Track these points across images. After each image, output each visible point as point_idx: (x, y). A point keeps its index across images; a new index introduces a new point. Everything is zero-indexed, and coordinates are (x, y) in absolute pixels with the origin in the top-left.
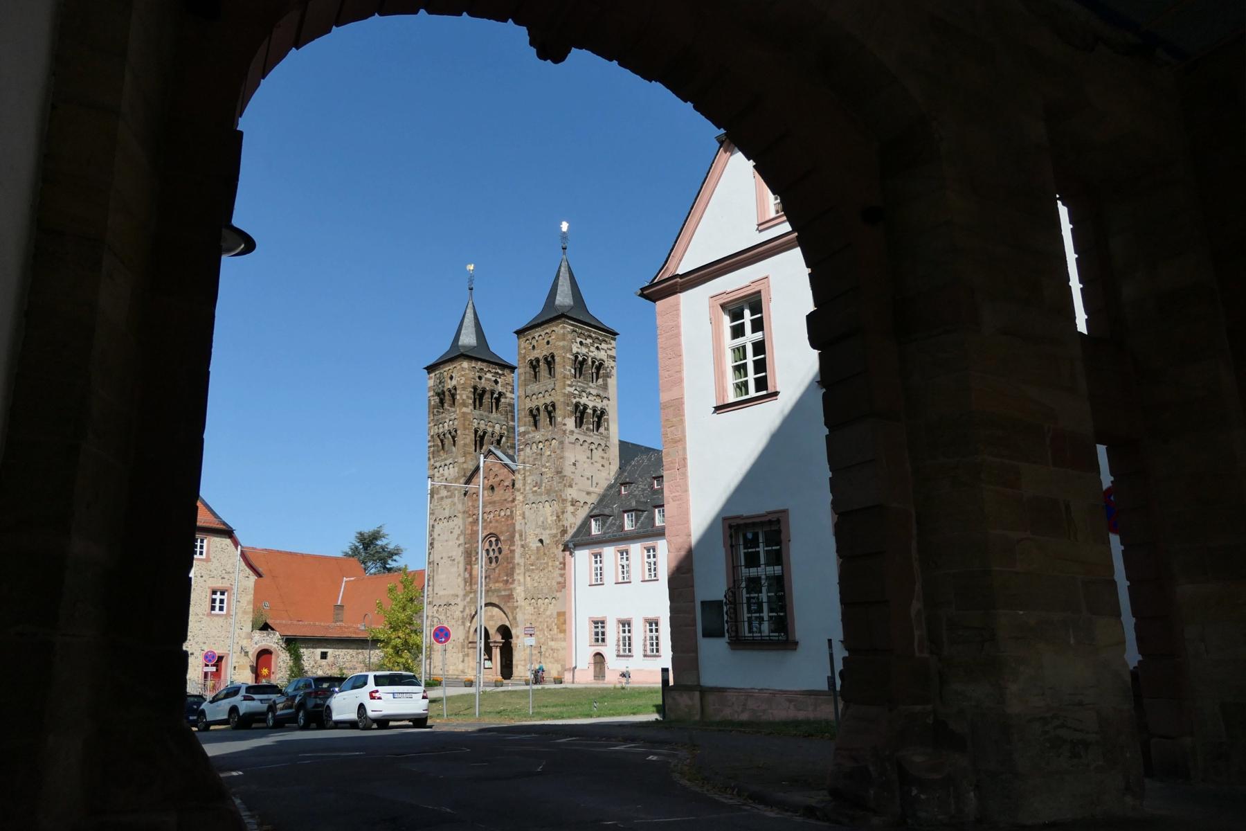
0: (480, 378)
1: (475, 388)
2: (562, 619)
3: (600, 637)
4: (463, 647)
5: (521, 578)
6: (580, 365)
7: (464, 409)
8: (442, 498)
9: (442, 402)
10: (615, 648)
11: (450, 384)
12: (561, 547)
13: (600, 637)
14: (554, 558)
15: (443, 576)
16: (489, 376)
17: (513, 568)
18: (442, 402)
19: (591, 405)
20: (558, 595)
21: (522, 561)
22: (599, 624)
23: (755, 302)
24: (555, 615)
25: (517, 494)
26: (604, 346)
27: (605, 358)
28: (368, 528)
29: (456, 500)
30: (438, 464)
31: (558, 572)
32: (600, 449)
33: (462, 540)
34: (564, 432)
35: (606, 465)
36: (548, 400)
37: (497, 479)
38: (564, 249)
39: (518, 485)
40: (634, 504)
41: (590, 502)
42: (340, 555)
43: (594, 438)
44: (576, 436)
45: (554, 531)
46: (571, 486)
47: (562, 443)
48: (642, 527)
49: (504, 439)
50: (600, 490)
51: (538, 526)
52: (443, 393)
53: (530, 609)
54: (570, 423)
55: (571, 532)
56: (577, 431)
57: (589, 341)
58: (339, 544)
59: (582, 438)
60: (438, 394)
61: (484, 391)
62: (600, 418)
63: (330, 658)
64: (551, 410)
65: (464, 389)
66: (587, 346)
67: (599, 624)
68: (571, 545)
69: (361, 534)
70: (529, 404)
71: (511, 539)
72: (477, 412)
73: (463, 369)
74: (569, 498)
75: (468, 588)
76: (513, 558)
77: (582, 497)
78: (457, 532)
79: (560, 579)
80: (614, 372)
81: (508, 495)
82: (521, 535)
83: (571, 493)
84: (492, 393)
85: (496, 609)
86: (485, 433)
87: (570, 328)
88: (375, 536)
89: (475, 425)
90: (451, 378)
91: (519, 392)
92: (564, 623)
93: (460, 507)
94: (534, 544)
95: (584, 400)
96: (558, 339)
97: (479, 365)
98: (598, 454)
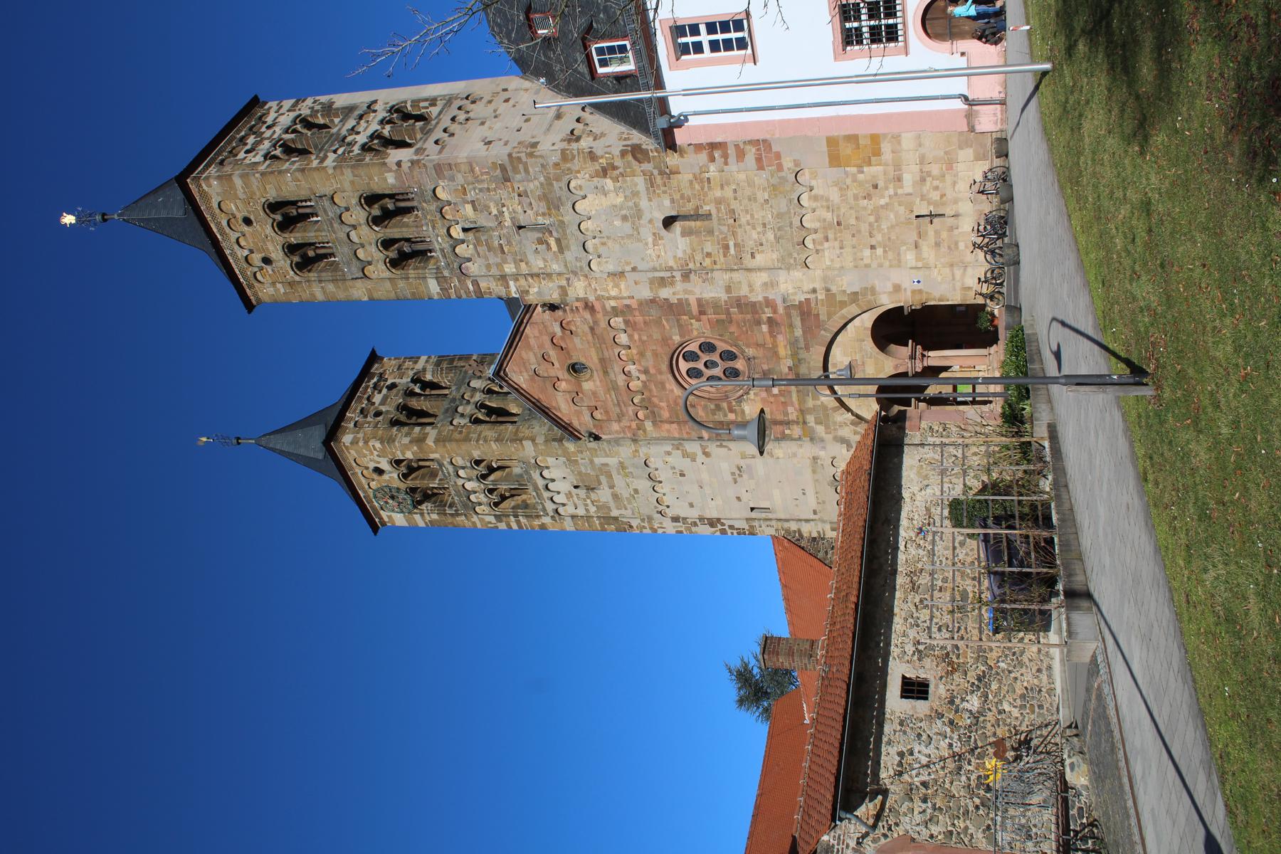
0: (378, 414)
1: (395, 423)
2: (846, 150)
7: (430, 442)
8: (616, 497)
9: (428, 496)
11: (392, 477)
12: (672, 159)
14: (701, 179)
15: (776, 493)
16: (377, 398)
17: (741, 304)
19: (375, 127)
20: (788, 163)
21: (722, 278)
24: (835, 173)
26: (269, 120)
28: (731, 691)
29: (613, 461)
33: (693, 447)
36: (358, 215)
37: (553, 354)
42: (763, 729)
45: (640, 182)
47: (439, 169)
51: (635, 235)
53: (830, 253)
55: (637, 137)
57: (251, 140)
58: (752, 732)
59: (438, 134)
60: (417, 504)
61: (403, 408)
62: (406, 116)
63: (927, 671)
69: (741, 702)
70: (379, 270)
71: (675, 310)
73: (355, 442)
75: (796, 431)
76: (716, 305)
78: (676, 459)
80: (324, 99)
81: (580, 322)
82: (662, 282)
83: (551, 144)
84: (410, 394)
85: (836, 352)
86: (483, 406)
87: (213, 170)
88: (743, 676)
90: (379, 471)
92: (853, 139)
93: (626, 451)
94: (677, 244)
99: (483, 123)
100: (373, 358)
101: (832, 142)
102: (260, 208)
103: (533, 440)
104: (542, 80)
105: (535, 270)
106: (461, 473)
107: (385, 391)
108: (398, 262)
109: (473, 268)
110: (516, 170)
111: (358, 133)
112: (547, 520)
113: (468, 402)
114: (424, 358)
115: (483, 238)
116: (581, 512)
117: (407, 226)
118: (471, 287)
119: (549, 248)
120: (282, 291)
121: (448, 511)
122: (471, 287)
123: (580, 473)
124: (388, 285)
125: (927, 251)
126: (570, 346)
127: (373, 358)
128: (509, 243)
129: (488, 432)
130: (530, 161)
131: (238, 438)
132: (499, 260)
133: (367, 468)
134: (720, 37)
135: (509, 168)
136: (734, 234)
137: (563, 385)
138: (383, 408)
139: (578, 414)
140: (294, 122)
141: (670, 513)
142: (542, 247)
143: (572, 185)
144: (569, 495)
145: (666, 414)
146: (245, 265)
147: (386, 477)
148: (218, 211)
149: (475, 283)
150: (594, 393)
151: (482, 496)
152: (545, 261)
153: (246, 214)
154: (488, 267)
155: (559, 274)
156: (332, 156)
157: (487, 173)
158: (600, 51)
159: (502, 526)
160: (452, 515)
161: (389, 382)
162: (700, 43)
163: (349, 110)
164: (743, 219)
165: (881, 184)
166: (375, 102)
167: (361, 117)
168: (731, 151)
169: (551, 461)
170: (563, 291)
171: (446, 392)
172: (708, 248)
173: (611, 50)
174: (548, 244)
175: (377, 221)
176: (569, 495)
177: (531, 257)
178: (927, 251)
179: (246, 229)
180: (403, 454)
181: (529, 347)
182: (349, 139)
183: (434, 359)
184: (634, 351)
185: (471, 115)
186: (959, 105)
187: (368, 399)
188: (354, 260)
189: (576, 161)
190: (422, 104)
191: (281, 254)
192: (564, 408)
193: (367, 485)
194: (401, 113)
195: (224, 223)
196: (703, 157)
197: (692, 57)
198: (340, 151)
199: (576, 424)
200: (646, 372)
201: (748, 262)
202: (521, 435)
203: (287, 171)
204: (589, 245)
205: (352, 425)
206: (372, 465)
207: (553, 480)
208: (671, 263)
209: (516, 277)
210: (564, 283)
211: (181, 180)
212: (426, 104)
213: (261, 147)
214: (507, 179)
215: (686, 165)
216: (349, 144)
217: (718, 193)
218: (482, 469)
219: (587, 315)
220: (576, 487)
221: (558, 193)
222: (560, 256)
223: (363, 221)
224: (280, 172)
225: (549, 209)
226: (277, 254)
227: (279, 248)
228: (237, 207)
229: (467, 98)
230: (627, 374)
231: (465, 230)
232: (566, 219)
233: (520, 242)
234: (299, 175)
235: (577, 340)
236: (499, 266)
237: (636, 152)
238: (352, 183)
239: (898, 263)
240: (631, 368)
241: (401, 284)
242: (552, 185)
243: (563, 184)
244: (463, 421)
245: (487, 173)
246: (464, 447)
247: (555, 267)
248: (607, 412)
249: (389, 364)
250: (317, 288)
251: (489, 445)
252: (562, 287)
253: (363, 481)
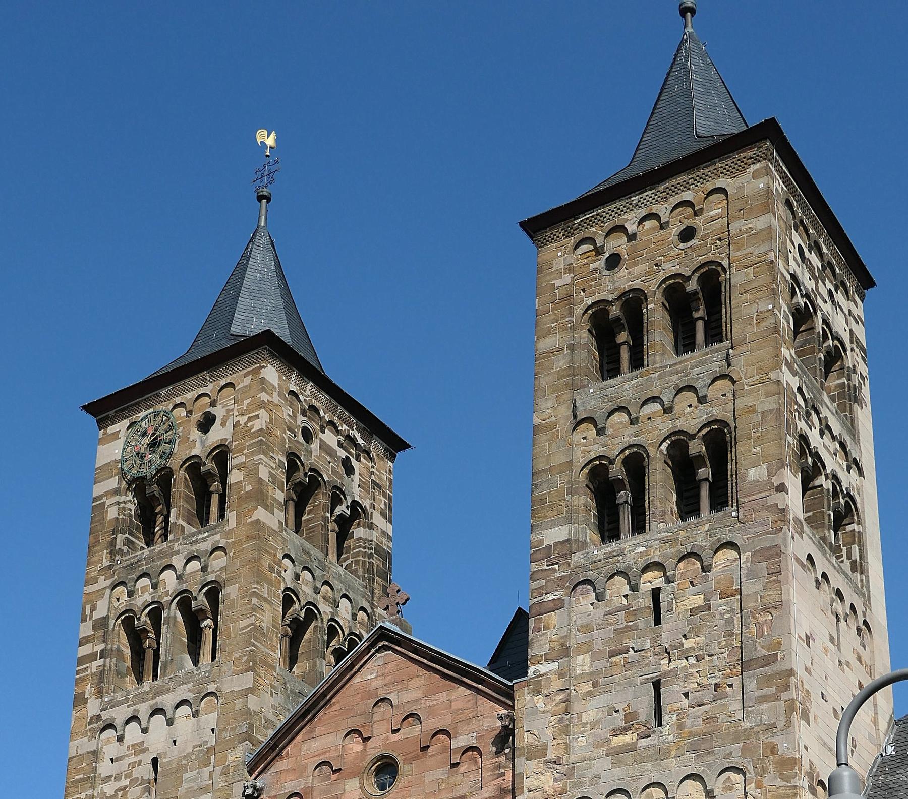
0: (307, 435)
1: (293, 462)
7: (261, 514)
11: (199, 445)
16: (330, 438)
26: (839, 297)
30: (119, 715)
36: (691, 417)
52: (165, 477)
57: (813, 258)
59: (822, 564)
60: (138, 485)
61: (314, 482)
65: (264, 447)
70: (587, 446)
80: (866, 392)
86: (311, 615)
87: (779, 186)
90: (207, 423)
97: (309, 392)
99: (832, 639)
100: (395, 445)
102: (711, 256)
104: (890, 749)
105: (576, 707)
106: (195, 565)
107: (342, 454)
108: (599, 479)
109: (585, 601)
110: (765, 681)
111: (822, 433)
112: (93, 707)
113: (317, 591)
114: (389, 529)
115: (641, 623)
118: (551, 597)
119: (617, 732)
120: (558, 283)
121: (120, 538)
122: (551, 597)
123: (182, 769)
124: (560, 459)
126: (430, 762)
127: (395, 445)
128: (628, 665)
130: (781, 705)
131: (269, 199)
132: (598, 646)
133: (213, 404)
135: (768, 670)
137: (355, 746)
138: (315, 446)
139: (299, 771)
140: (836, 338)
142: (619, 720)
143: (733, 776)
144: (140, 748)
146: (608, 225)
147: (195, 434)
148: (710, 186)
149: (558, 605)
151: (147, 597)
152: (594, 725)
153: (700, 233)
154: (586, 628)
155: (567, 747)
156: (794, 382)
157: (761, 634)
159: (86, 629)
160: (113, 543)
161: (354, 462)
163: (852, 426)
166: (861, 473)
167: (843, 445)
169: (210, 719)
174: (624, 731)
177: (602, 700)
179: (675, 231)
180: (239, 467)
181: (430, 692)
183: (387, 545)
185: (843, 623)
187: (331, 423)
188: (610, 406)
189: (779, 782)
190: (855, 549)
191: (626, 286)
193: (180, 404)
194: (845, 514)
195: (687, 196)
199: (280, 765)
202: (262, 671)
205: (293, 388)
206: (219, 412)
207: (170, 722)
211: (768, 133)
212: (856, 555)
213: (807, 275)
214: (745, 666)
216: (808, 414)
218: (201, 601)
220: (155, 762)
221: (720, 751)
222: (601, 751)
223: (680, 425)
225: (691, 734)
226: (625, 279)
227: (637, 284)
228: (713, 219)
231: (656, 593)
232: (671, 762)
233: (631, 684)
234: (769, 323)
235: (441, 773)
236: (587, 647)
238: (752, 410)
241: (561, 481)
242: (736, 740)
243: (737, 760)
244: (288, 576)
245: (761, 634)
246: (245, 571)
247: (581, 743)
249: (383, 469)
250: (565, 342)
251: (252, 615)
252: (544, 750)
253: (190, 395)
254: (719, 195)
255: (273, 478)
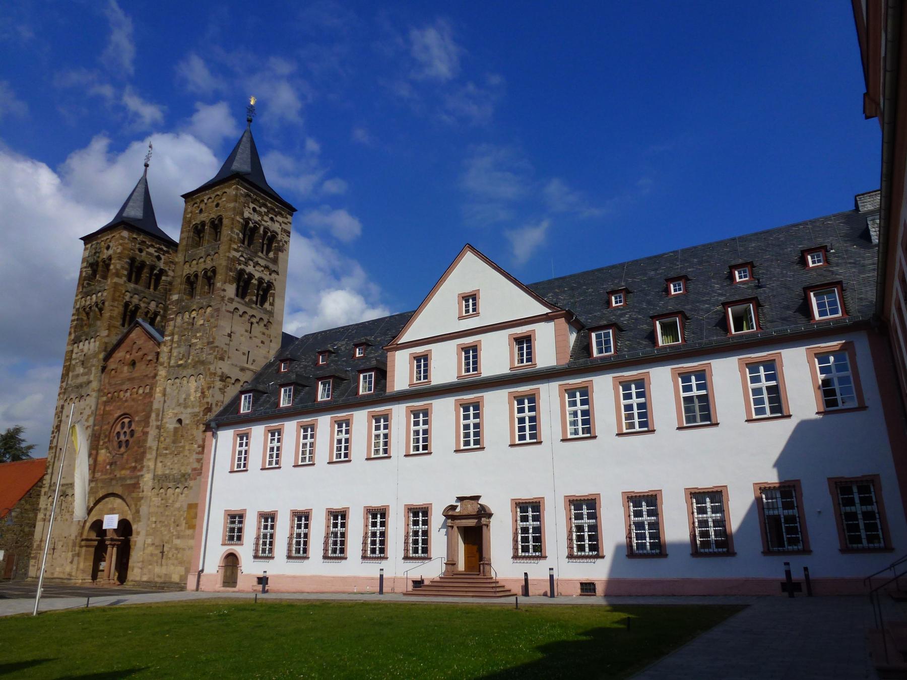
1: (133, 260)
3: (234, 534)
4: (74, 545)
5: (151, 464)
6: (249, 232)
7: (116, 280)
8: (78, 376)
9: (95, 273)
10: (253, 547)
11: (105, 254)
12: (202, 428)
13: (234, 534)
14: (193, 440)
16: (151, 250)
17: (144, 453)
18: (95, 273)
22: (236, 519)
23: (386, 418)
25: (160, 368)
26: (279, 218)
27: (279, 231)
31: (195, 456)
32: (262, 324)
33: (91, 420)
34: (223, 298)
35: (267, 342)
36: (209, 264)
37: (140, 353)
38: (250, 121)
39: (163, 358)
40: (294, 377)
41: (243, 379)
43: (256, 311)
44: (235, 305)
45: (197, 410)
46: (222, 359)
47: (218, 310)
48: (301, 401)
49: (159, 318)
50: (257, 367)
53: (156, 500)
54: (231, 290)
55: (216, 410)
56: (237, 299)
57: (263, 210)
59: (242, 309)
61: (143, 264)
64: (210, 277)
66: (260, 214)
67: (236, 519)
68: (213, 425)
70: (187, 270)
71: (146, 421)
72: (132, 285)
73: (123, 238)
74: (219, 372)
76: (145, 441)
77: (235, 374)
78: (88, 412)
79: (196, 465)
81: (150, 371)
82: (158, 415)
83: (224, 367)
85: (119, 501)
87: (243, 191)
89: (127, 298)
90: (108, 248)
91: (179, 268)
92: (195, 517)
94: (171, 425)
95: (250, 269)
96: (228, 201)
97: (141, 238)
98: (258, 329)
101: (196, 505)
103: (108, 336)
107: (156, 254)
116: (74, 356)
117: (202, 288)
125: (150, 549)
129: (118, 310)
134: (472, 430)
136: (171, 454)
141: (66, 404)
145: (107, 409)
149: (172, 319)
150: (122, 372)
158: (370, 376)
162: (418, 425)
164: (176, 459)
165: (178, 528)
168: (200, 456)
170: (162, 364)
171: (152, 287)
172: (168, 440)
173: (370, 383)
175: (206, 273)
176: (82, 351)
178: (150, 549)
182: (251, 263)
184: (135, 396)
186: (200, 568)
192: (120, 354)
195: (219, 193)
196: (200, 442)
197: (412, 420)
198: (242, 259)
199: (111, 360)
200: (126, 401)
201: (159, 459)
203: (232, 232)
204: (177, 381)
206: (111, 244)
208: (165, 420)
209: (172, 341)
210: (166, 365)
215: (198, 433)
217: (187, 448)
219: (152, 374)
224: (232, 228)
229: (269, 322)
230: (126, 391)
235: (144, 367)
237: (209, 410)
239: (147, 535)
240: (128, 394)
241: (179, 280)
243: (202, 371)
248: (114, 377)
251: (113, 311)
254: (161, 226)
255: (123, 268)
